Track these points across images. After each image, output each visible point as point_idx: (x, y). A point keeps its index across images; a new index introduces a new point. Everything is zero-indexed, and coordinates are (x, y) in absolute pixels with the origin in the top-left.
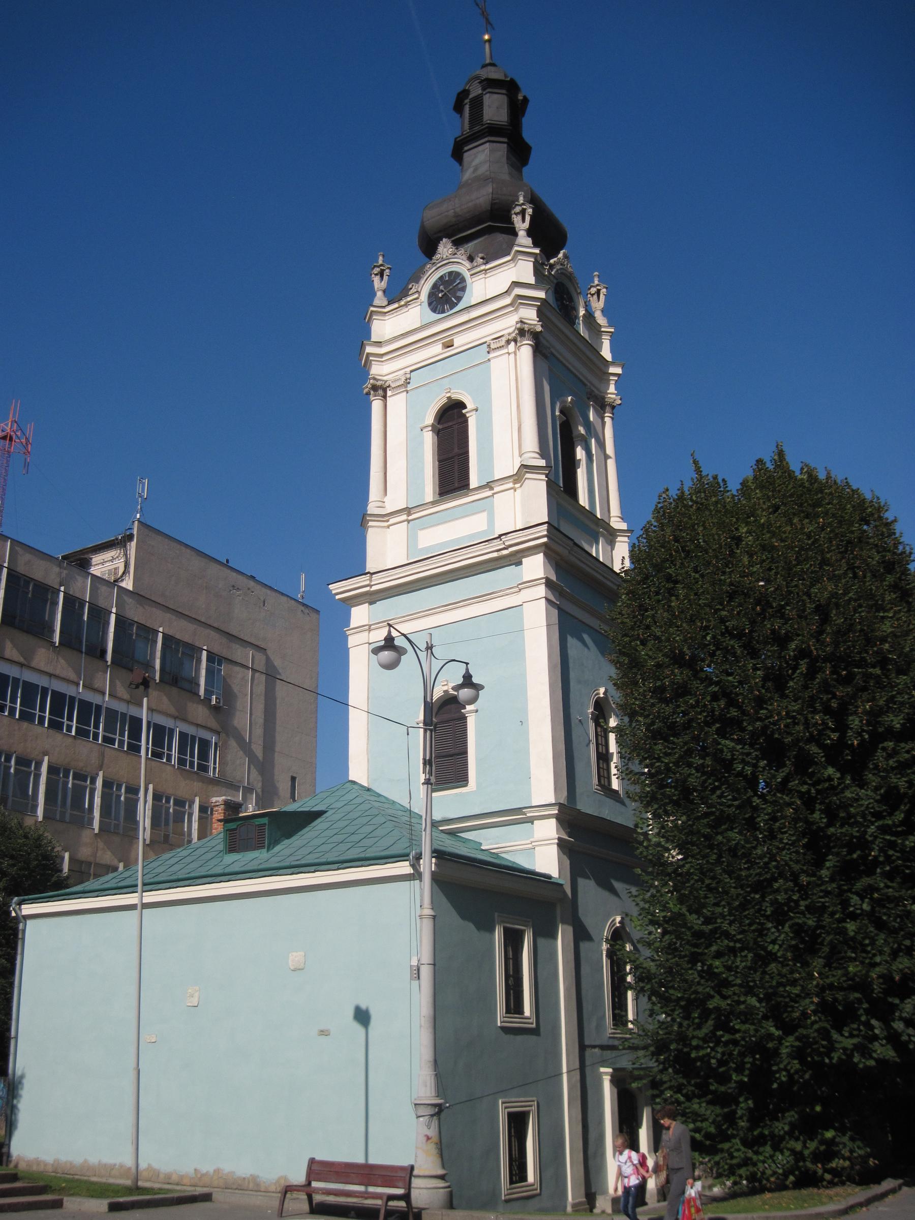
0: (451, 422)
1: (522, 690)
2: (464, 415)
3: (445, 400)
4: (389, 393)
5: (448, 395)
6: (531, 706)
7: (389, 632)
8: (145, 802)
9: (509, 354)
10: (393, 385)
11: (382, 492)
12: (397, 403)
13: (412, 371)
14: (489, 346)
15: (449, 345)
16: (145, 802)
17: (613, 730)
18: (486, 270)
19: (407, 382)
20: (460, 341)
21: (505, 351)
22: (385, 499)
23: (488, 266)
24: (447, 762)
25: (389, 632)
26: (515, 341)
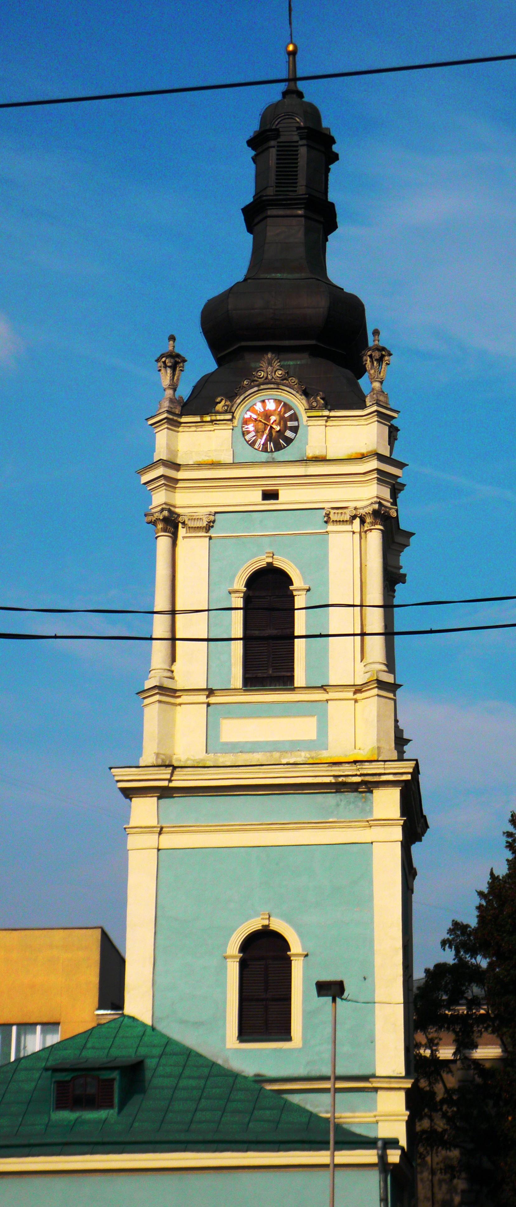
0: (268, 600)
1: (368, 942)
2: (292, 591)
3: (263, 564)
4: (182, 532)
5: (270, 560)
6: (378, 960)
7: (395, 695)
8: (361, 1117)
9: (354, 533)
10: (191, 524)
11: (169, 660)
12: (193, 550)
13: (216, 513)
14: (327, 515)
15: (270, 495)
16: (361, 1117)
17: (469, 1009)
18: (329, 417)
19: (208, 527)
20: (288, 496)
21: (348, 527)
22: (174, 668)
23: (332, 414)
24: (264, 1009)
25: (395, 695)
26: (363, 522)
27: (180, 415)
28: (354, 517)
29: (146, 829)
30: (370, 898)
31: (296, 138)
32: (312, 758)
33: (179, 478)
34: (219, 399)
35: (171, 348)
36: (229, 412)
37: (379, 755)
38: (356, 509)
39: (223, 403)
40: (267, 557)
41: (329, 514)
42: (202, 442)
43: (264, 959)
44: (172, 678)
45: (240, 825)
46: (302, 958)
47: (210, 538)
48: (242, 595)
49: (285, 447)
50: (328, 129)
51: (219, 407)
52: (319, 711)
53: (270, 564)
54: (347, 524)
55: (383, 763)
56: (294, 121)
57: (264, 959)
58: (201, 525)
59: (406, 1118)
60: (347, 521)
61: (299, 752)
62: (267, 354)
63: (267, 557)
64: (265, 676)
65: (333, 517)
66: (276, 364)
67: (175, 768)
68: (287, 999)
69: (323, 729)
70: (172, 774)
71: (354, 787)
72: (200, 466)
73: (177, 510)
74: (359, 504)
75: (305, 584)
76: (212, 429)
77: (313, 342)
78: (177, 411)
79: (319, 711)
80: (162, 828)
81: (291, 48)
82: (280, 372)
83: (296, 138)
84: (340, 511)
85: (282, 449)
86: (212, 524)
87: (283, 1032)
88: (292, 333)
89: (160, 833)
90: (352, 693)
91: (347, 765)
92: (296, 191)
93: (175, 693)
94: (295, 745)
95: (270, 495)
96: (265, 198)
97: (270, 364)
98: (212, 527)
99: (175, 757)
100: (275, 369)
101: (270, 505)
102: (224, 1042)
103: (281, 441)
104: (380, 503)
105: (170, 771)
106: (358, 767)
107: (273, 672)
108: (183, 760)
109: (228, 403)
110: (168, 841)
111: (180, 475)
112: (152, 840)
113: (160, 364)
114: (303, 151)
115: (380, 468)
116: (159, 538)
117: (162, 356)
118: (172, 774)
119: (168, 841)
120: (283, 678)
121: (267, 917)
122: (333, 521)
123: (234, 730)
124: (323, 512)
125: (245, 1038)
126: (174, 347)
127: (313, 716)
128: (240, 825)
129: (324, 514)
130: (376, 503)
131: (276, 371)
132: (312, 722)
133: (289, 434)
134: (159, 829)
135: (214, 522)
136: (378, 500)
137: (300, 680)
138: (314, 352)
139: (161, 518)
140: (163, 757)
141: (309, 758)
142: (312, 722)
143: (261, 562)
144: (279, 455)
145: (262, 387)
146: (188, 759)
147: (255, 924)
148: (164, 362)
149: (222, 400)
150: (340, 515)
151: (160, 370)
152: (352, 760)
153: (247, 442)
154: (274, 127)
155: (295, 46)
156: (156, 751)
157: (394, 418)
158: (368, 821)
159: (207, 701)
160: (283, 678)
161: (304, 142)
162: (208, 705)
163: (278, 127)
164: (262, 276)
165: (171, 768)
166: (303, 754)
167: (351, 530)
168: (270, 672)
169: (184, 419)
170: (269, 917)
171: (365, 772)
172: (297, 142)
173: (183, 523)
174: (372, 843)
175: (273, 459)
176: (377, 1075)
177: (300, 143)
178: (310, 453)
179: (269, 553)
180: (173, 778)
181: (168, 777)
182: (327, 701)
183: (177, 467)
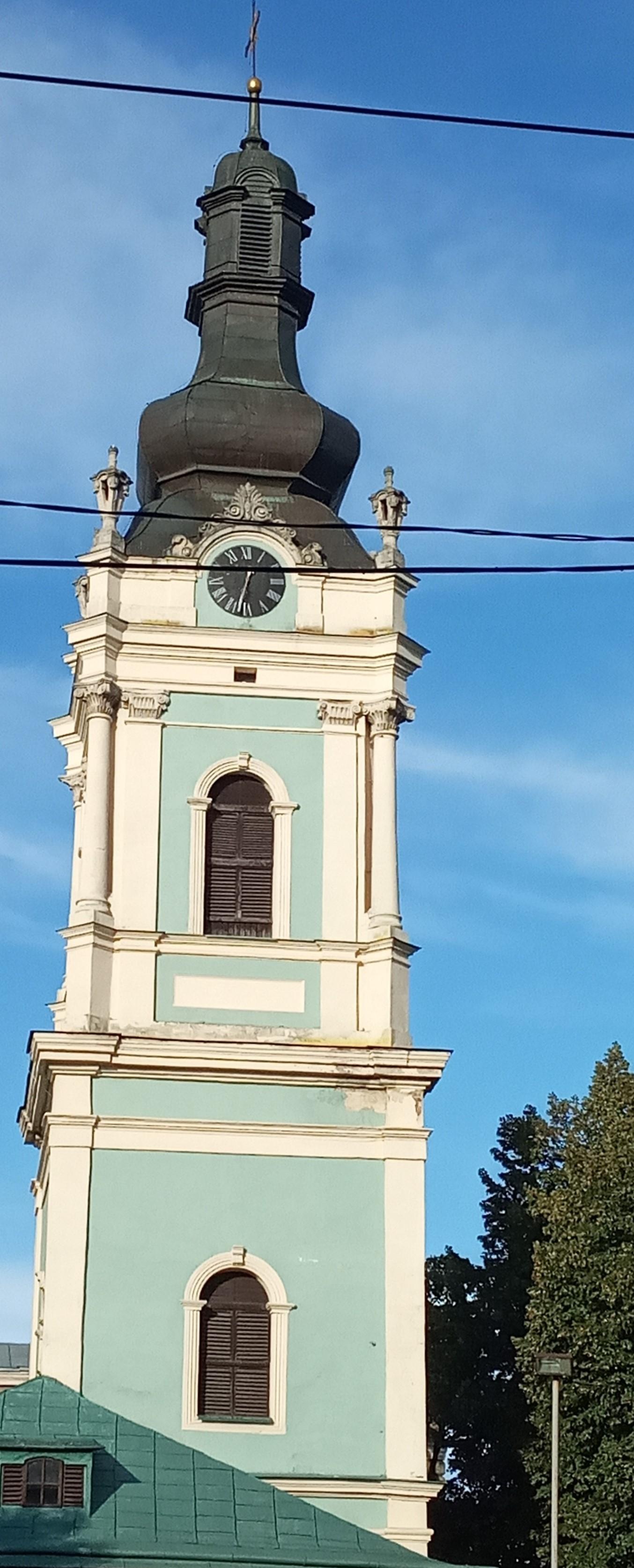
3: (234, 767)
9: (358, 736)
12: (137, 739)
13: (171, 692)
20: (268, 678)
27: (126, 555)
28: (360, 715)
29: (75, 1120)
30: (381, 1233)
31: (270, 203)
32: (300, 1038)
33: (124, 640)
34: (177, 539)
35: (112, 464)
36: (193, 558)
37: (393, 1043)
38: (361, 704)
39: (183, 544)
40: (241, 758)
41: (325, 708)
42: (166, 594)
43: (233, 1308)
44: (109, 913)
45: (205, 1123)
46: (288, 1312)
47: (164, 726)
48: (205, 807)
49: (266, 612)
50: (305, 195)
51: (177, 550)
52: (309, 974)
53: (243, 769)
54: (348, 724)
55: (406, 1052)
56: (265, 180)
57: (233, 1308)
58: (150, 707)
59: (429, 1539)
60: (349, 719)
61: (282, 1029)
62: (244, 485)
63: (241, 758)
64: (232, 920)
65: (331, 713)
66: (256, 500)
67: (121, 1037)
68: (263, 1366)
69: (312, 997)
70: (117, 1047)
71: (361, 1082)
72: (152, 626)
73: (118, 684)
74: (365, 699)
75: (291, 800)
76: (168, 578)
77: (297, 475)
78: (121, 549)
79: (309, 974)
80: (98, 1120)
81: (253, 84)
82: (262, 511)
83: (270, 203)
84: (340, 705)
85: (262, 614)
86: (164, 707)
87: (258, 1410)
88: (248, 462)
89: (95, 1126)
90: (353, 954)
91: (357, 1051)
92: (266, 272)
93: (114, 935)
94: (280, 1019)
95: (244, 676)
96: (226, 277)
97: (248, 498)
98: (166, 710)
99: (111, 1022)
100: (254, 507)
101: (244, 688)
102: (186, 1426)
103: (261, 603)
104: (398, 700)
105: (115, 1043)
106: (373, 1055)
107: (243, 916)
108: (122, 1027)
109: (190, 545)
110: (105, 1138)
111: (126, 636)
112: (83, 1135)
113: (98, 483)
114: (277, 220)
115: (400, 653)
116: (91, 721)
117: (101, 473)
118: (117, 1047)
119: (105, 1138)
120: (259, 927)
121: (242, 1252)
122: (331, 718)
123: (193, 992)
124: (318, 705)
125: (208, 1417)
126: (116, 462)
127: (301, 980)
128: (205, 1123)
129: (318, 708)
130: (392, 699)
131: (256, 509)
132: (298, 988)
133: (271, 594)
134: (94, 1121)
135: (168, 705)
136: (396, 696)
137: (280, 926)
138: (297, 487)
139: (100, 692)
140: (97, 1021)
141: (294, 1038)
142: (298, 988)
143: (235, 764)
144: (257, 622)
145: (238, 528)
146: (129, 1028)
147: (227, 1260)
148: (105, 482)
149: (182, 540)
150: (339, 710)
151: (96, 492)
152: (365, 1045)
153: (215, 600)
154: (239, 185)
155: (259, 82)
156: (88, 1012)
157: (412, 586)
158: (380, 1130)
159: (156, 949)
160: (259, 927)
161: (279, 208)
162: (158, 953)
163: (243, 184)
164: (223, 379)
165: (117, 1038)
166: (287, 1031)
167: (354, 732)
168: (239, 915)
169: (131, 561)
170: (245, 1251)
171: (381, 1062)
172: (269, 207)
173: (127, 702)
174: (384, 1160)
175: (251, 626)
176: (389, 1477)
177: (275, 209)
178: (301, 624)
179: (245, 753)
180: (119, 1052)
181: (112, 1050)
182: (321, 961)
183: (123, 625)
